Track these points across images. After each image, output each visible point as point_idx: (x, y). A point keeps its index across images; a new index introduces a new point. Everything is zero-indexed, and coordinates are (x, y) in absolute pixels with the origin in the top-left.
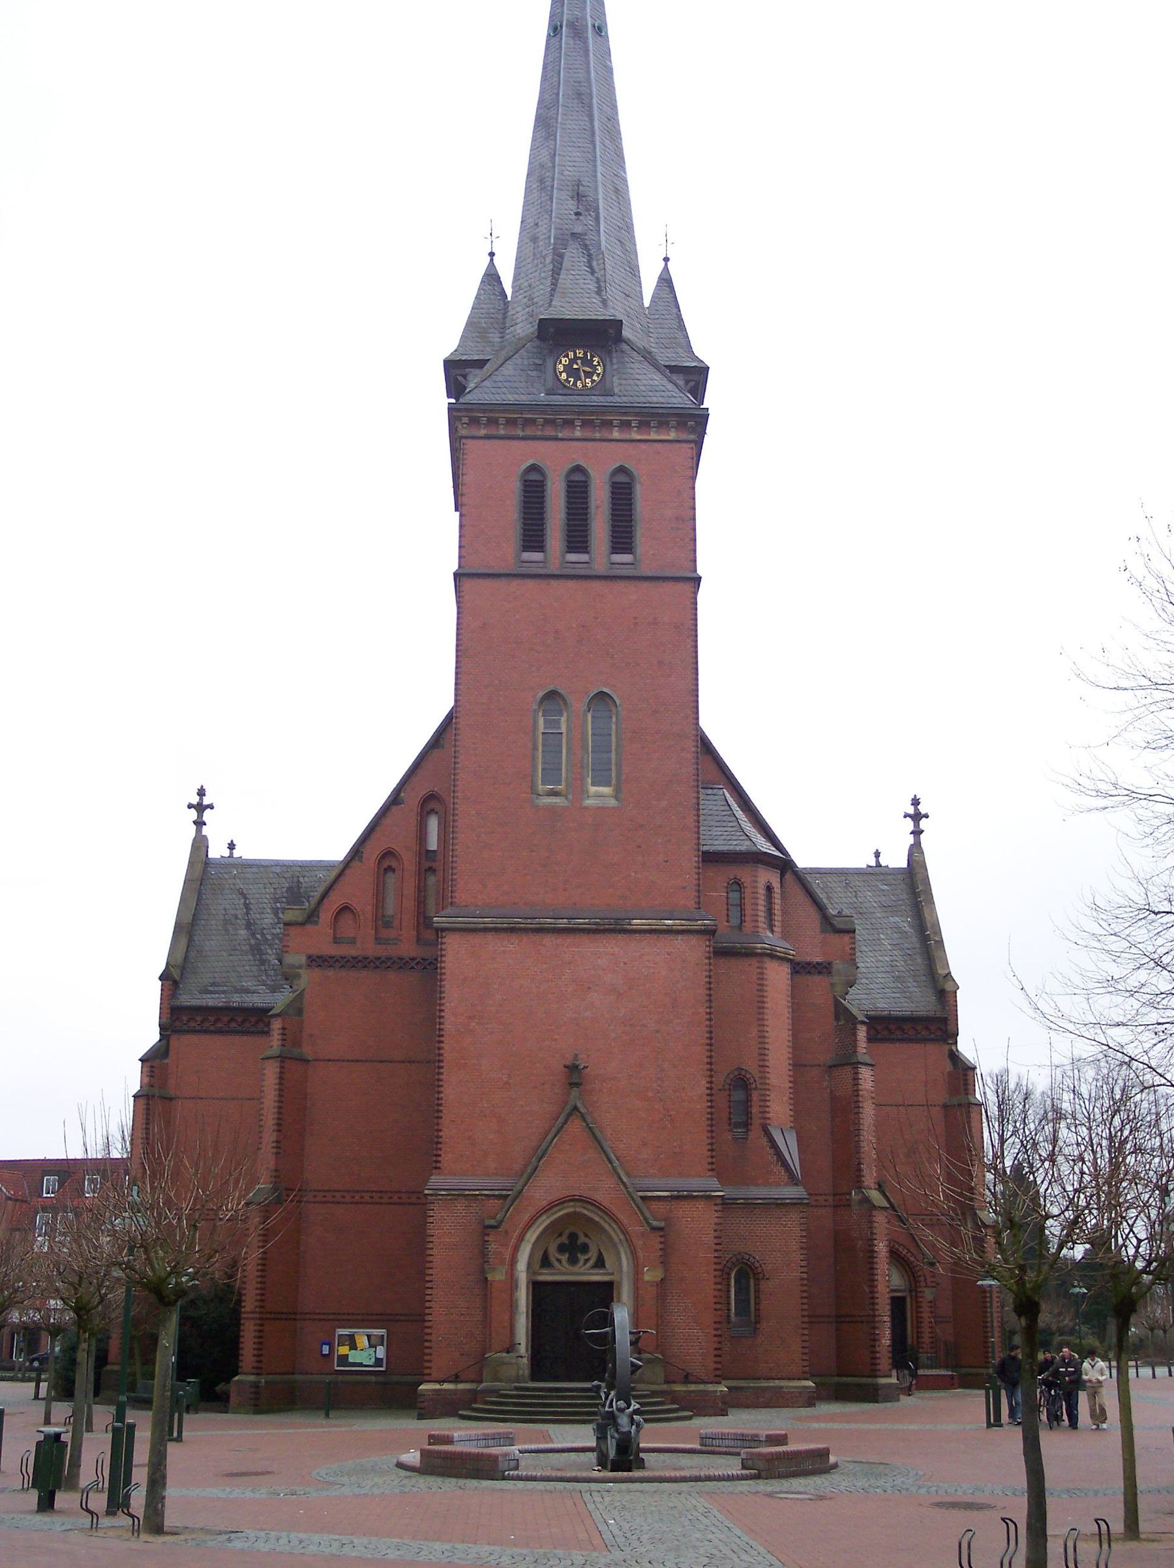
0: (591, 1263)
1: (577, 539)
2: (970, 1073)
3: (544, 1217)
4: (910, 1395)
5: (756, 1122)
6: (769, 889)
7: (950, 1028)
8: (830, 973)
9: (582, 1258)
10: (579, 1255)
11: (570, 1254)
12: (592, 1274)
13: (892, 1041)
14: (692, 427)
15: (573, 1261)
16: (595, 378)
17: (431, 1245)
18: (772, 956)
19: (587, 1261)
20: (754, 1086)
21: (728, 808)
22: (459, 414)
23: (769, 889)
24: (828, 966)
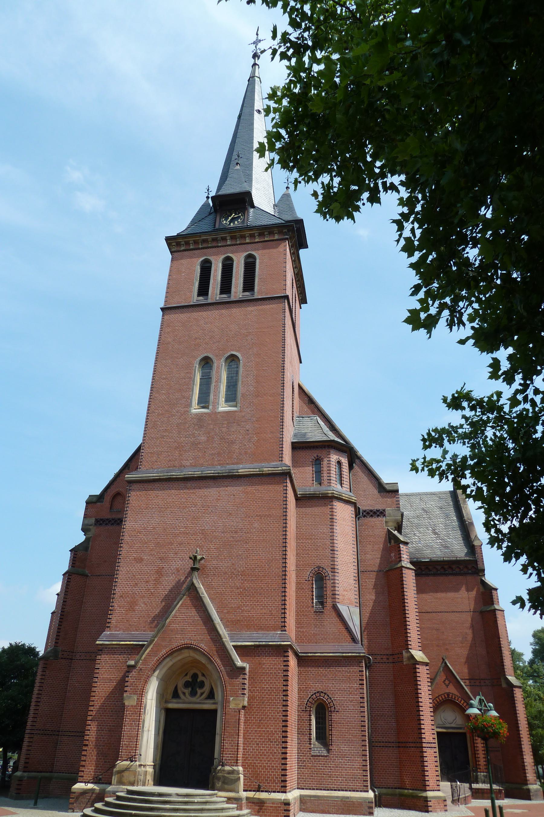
0: (204, 696)
1: (226, 288)
2: (493, 592)
3: (168, 659)
4: (446, 811)
5: (329, 601)
6: (339, 463)
7: (480, 566)
8: (385, 515)
9: (199, 691)
10: (197, 689)
11: (192, 689)
12: (204, 703)
13: (446, 575)
14: (286, 232)
15: (193, 693)
16: (239, 220)
17: (96, 680)
18: (340, 499)
19: (202, 694)
20: (328, 578)
21: (318, 424)
22: (171, 241)
23: (339, 463)
24: (383, 511)
